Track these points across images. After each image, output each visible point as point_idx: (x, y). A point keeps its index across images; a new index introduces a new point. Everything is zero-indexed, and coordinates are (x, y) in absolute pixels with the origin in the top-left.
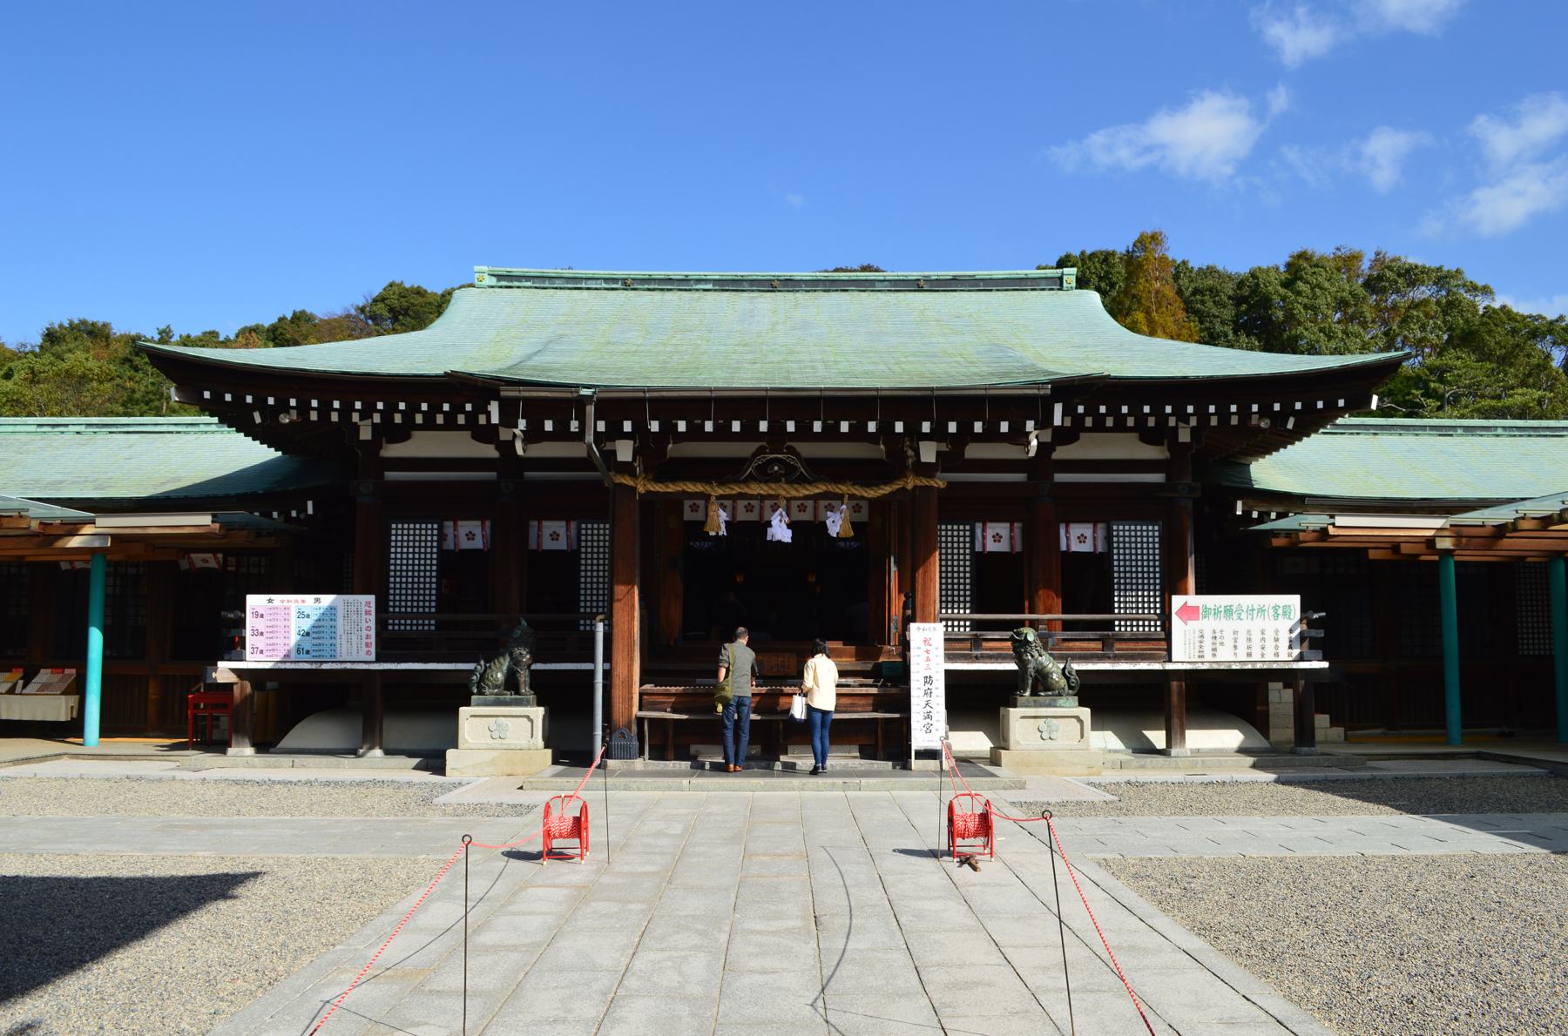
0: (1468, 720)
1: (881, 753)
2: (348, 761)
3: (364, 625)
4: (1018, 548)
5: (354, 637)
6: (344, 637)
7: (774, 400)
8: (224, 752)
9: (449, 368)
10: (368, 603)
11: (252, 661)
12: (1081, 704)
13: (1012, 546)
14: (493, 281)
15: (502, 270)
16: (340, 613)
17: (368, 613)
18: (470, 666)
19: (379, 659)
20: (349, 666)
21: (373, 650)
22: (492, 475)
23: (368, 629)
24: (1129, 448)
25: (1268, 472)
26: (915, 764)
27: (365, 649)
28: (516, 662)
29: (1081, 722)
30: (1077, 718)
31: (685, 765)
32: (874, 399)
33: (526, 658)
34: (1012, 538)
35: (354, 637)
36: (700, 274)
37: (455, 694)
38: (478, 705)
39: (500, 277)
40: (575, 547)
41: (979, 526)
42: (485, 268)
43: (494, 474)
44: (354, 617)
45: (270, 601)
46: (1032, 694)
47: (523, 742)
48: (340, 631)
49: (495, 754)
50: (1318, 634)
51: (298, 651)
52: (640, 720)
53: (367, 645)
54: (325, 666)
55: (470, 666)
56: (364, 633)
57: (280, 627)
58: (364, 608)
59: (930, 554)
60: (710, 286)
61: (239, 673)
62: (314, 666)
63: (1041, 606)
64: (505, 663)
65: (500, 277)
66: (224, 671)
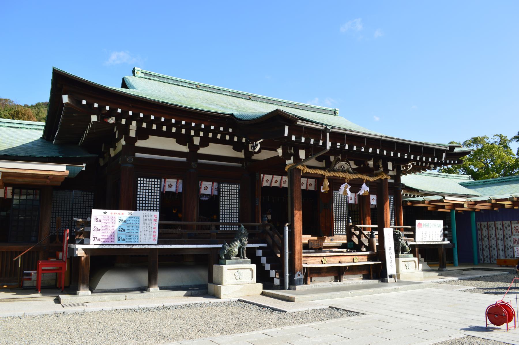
0: (459, 262)
1: (372, 277)
2: (137, 295)
3: (153, 226)
4: (357, 202)
5: (148, 232)
6: (143, 232)
7: (383, 141)
8: (75, 294)
9: (230, 111)
10: (155, 216)
11: (94, 244)
12: (252, 263)
13: (355, 201)
14: (143, 75)
15: (147, 72)
16: (141, 220)
17: (155, 220)
18: (220, 246)
19: (159, 243)
20: (147, 247)
21: (156, 238)
22: (184, 159)
23: (155, 228)
24: (169, 144)
25: (407, 180)
26: (389, 280)
27: (152, 238)
28: (242, 244)
29: (252, 271)
30: (251, 269)
31: (376, 281)
32: (408, 145)
33: (246, 243)
34: (355, 199)
35: (148, 232)
36: (225, 89)
37: (218, 258)
38: (229, 264)
39: (145, 74)
40: (216, 193)
41: (163, 180)
42: (139, 69)
43: (185, 159)
44: (148, 222)
45: (105, 213)
46: (402, 253)
47: (250, 281)
48: (141, 229)
49: (242, 286)
50: (447, 233)
51: (119, 239)
52: (304, 268)
53: (154, 236)
54: (135, 247)
55: (220, 246)
56: (153, 230)
57: (106, 226)
58: (153, 218)
59: (387, 201)
60: (228, 94)
61: (85, 250)
62: (129, 247)
63: (367, 222)
64: (238, 244)
65: (145, 74)
66: (80, 250)
